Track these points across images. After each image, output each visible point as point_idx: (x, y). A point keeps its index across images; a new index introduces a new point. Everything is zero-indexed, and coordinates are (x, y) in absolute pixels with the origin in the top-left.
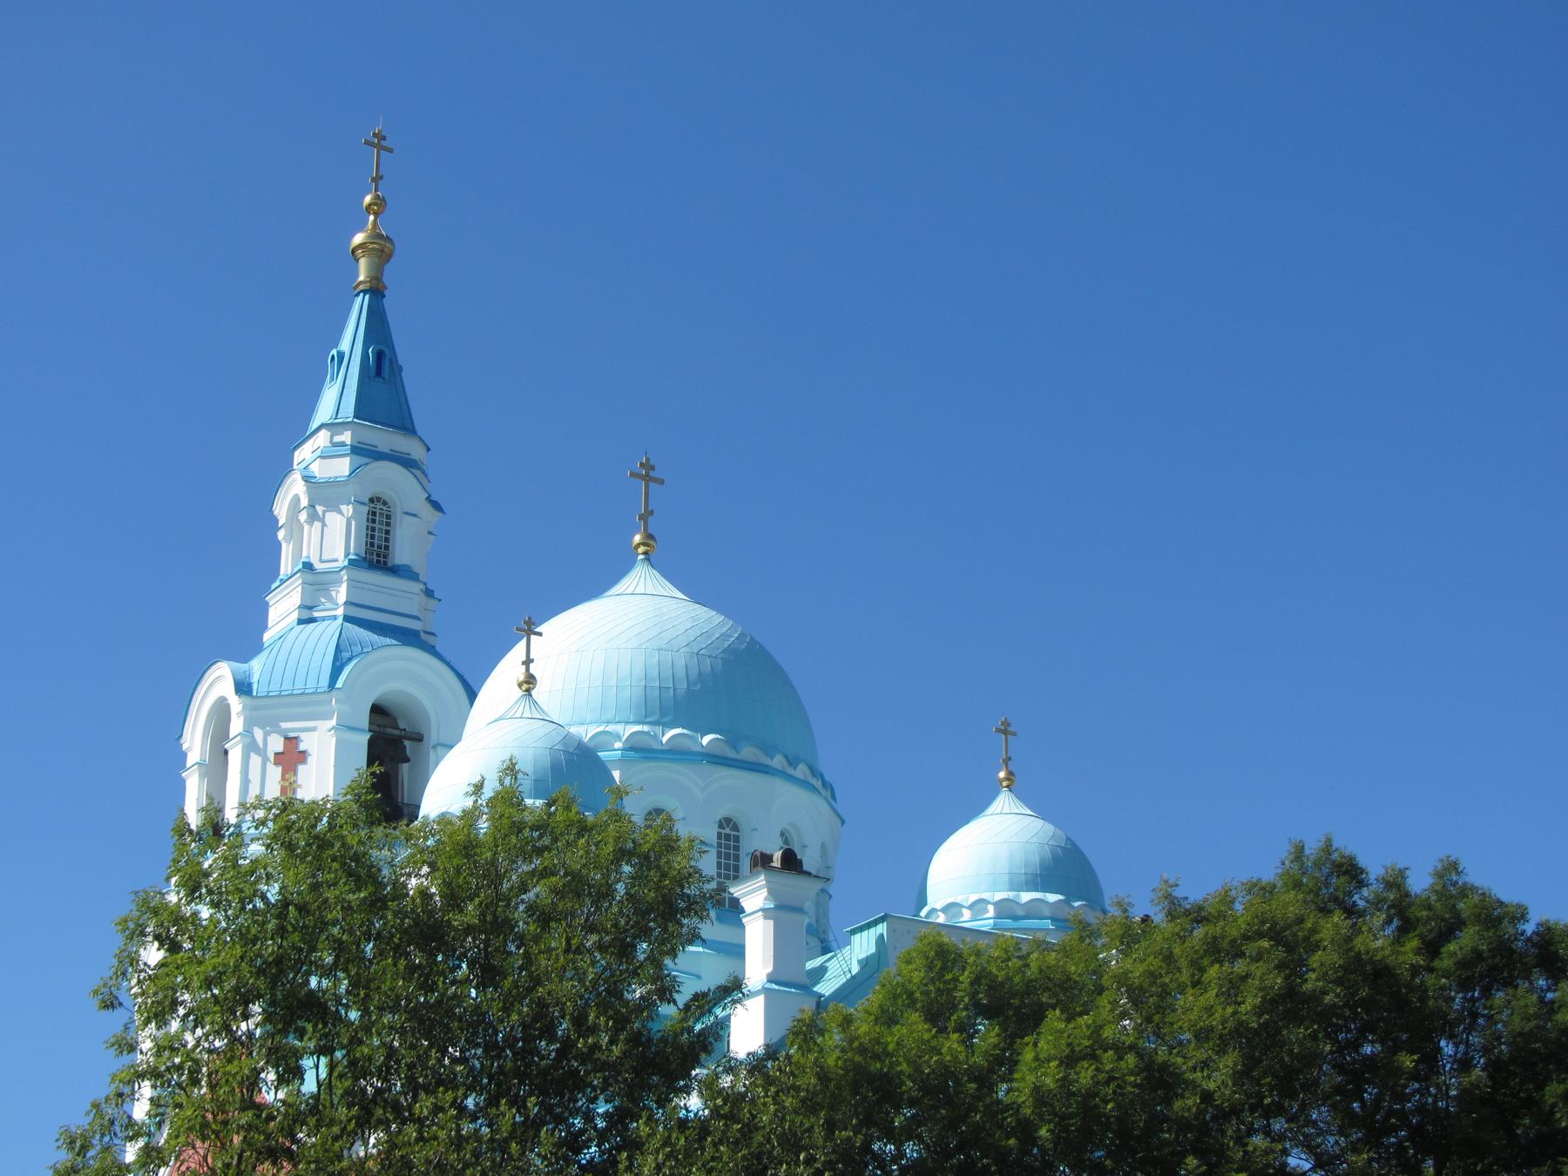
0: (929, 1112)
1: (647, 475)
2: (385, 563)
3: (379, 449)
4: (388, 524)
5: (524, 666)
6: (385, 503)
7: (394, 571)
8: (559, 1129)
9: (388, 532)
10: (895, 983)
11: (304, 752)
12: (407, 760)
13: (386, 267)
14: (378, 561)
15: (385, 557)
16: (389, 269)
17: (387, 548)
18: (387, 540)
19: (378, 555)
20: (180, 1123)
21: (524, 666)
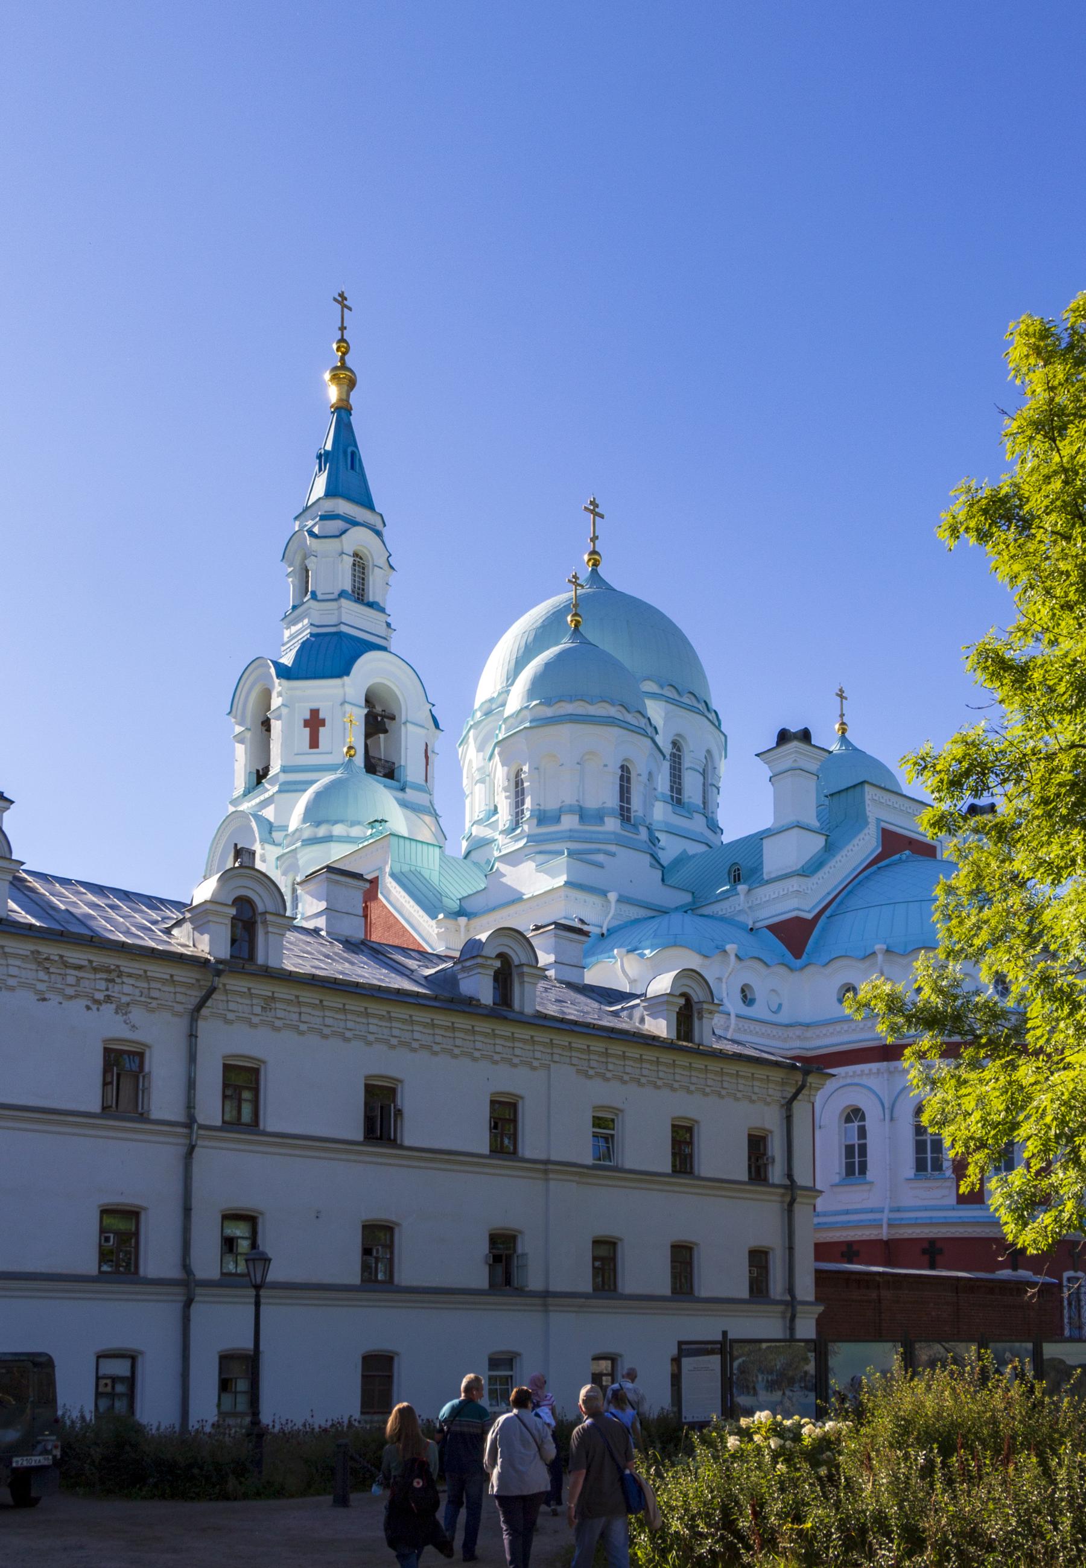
0: (977, 1115)
1: (594, 510)
2: (363, 600)
3: (357, 520)
4: (363, 573)
5: (308, 730)
6: (361, 558)
7: (371, 605)
8: (1060, 1235)
9: (363, 579)
10: (1057, 1004)
11: (305, 726)
12: (385, 731)
13: (352, 393)
14: (358, 599)
15: (362, 596)
16: (354, 395)
17: (363, 590)
18: (363, 584)
19: (358, 594)
20: (438, 1039)
21: (308, 730)
